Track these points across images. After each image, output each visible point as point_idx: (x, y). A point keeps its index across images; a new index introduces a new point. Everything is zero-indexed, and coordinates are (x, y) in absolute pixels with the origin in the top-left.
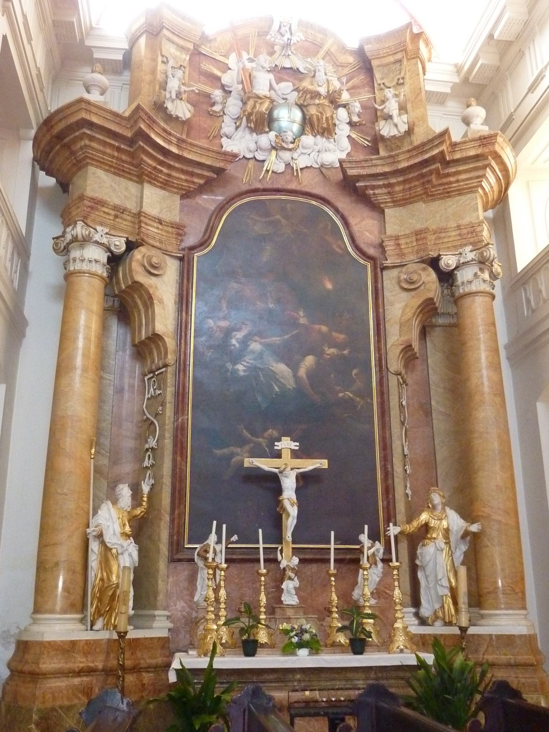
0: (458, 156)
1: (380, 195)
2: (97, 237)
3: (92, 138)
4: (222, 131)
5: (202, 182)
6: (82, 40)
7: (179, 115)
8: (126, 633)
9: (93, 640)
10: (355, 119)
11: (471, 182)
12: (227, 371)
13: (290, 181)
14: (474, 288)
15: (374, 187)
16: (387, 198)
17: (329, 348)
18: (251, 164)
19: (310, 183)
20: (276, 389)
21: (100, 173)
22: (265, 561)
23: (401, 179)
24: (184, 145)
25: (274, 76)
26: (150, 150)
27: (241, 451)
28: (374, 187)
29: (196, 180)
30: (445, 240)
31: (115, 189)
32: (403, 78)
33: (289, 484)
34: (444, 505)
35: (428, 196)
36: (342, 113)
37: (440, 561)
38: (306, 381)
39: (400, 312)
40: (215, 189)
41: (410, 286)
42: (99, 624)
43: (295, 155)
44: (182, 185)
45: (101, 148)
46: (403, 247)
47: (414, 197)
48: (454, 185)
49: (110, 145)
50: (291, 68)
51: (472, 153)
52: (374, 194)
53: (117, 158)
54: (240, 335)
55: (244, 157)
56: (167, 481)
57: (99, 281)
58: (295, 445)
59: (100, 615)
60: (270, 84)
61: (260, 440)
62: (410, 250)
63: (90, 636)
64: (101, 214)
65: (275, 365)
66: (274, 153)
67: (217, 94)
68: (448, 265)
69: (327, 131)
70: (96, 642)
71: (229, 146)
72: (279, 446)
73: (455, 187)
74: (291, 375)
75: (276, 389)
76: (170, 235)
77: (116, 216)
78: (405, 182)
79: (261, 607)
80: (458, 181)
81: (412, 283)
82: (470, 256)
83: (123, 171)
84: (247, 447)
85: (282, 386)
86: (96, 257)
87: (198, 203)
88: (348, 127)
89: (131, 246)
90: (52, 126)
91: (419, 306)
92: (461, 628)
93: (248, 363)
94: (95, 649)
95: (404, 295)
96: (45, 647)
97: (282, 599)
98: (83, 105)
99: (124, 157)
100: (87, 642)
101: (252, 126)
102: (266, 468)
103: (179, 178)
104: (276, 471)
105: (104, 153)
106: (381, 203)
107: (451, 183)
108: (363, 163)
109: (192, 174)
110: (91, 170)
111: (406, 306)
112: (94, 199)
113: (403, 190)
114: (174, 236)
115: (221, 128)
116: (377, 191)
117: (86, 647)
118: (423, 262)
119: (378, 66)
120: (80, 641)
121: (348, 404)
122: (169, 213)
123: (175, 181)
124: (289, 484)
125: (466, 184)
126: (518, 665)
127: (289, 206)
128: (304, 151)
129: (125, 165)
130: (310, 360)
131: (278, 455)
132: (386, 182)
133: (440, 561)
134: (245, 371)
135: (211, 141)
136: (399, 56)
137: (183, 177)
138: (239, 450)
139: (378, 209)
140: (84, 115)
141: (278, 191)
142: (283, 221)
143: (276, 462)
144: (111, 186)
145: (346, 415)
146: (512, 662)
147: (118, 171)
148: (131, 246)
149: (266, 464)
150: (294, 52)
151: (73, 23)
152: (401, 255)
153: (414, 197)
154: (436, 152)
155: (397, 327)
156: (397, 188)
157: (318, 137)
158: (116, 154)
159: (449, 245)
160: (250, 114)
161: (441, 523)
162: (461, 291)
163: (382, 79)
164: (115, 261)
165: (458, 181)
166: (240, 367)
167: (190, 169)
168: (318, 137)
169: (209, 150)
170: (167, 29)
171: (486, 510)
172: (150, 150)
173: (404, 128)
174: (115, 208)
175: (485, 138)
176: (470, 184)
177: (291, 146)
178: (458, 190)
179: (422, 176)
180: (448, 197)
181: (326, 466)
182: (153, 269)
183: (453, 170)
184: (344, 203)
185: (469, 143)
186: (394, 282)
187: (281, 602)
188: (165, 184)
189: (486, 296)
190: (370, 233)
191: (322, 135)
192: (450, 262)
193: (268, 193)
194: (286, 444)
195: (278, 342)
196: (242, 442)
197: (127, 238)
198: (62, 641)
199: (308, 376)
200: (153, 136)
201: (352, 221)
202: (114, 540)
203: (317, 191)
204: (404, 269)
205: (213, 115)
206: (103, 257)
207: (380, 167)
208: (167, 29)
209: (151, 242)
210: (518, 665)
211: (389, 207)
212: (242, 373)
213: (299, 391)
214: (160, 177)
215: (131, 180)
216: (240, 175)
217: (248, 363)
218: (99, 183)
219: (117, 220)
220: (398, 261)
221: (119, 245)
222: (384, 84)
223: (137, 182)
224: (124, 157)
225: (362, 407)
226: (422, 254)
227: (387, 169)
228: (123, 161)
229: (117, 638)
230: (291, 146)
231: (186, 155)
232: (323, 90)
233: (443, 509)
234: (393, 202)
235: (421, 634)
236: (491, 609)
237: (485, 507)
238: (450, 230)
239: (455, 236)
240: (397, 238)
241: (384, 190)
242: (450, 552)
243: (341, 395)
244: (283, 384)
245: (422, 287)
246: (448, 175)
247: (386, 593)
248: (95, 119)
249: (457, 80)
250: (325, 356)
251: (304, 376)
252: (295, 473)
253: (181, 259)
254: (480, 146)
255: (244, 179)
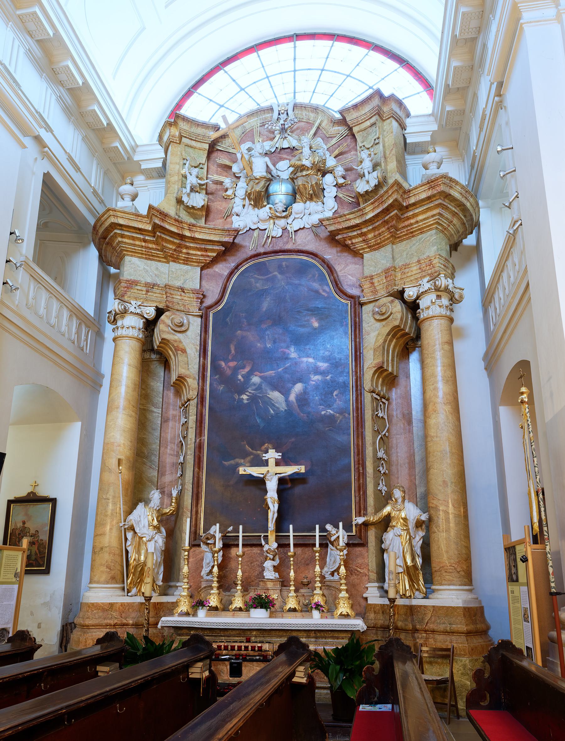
0: (412, 200)
1: (358, 243)
2: (132, 309)
3: (122, 236)
4: (233, 211)
5: (215, 254)
6: (130, 158)
7: (194, 205)
8: (150, 598)
9: (127, 603)
10: (341, 181)
11: (428, 221)
12: (235, 400)
13: (287, 242)
14: (431, 313)
15: (351, 238)
16: (363, 245)
17: (315, 375)
18: (256, 233)
19: (306, 241)
20: (272, 412)
21: (135, 260)
22: (243, 545)
23: (371, 227)
24: (194, 229)
25: (270, 159)
26: (168, 238)
27: (244, 462)
28: (351, 238)
29: (210, 254)
30: (409, 274)
31: (147, 271)
32: (378, 138)
33: (272, 486)
34: (404, 499)
35: (395, 238)
36: (329, 178)
37: (399, 546)
38: (296, 404)
39: (374, 339)
40: (228, 258)
41: (383, 317)
42: (134, 591)
43: (290, 220)
44: (200, 260)
45: (131, 242)
46: (376, 285)
47: (384, 241)
48: (415, 226)
49: (139, 239)
50: (289, 148)
51: (423, 196)
52: (352, 243)
53: (146, 247)
54: (245, 371)
55: (250, 228)
56: (189, 487)
57: (135, 342)
58: (278, 456)
59: (135, 585)
60: (267, 166)
61: (259, 452)
62: (381, 287)
63: (127, 600)
64: (136, 291)
65: (271, 393)
66: (272, 221)
67: (227, 181)
68: (409, 296)
69: (317, 194)
70: (130, 605)
71: (237, 223)
72: (266, 456)
73: (416, 227)
74: (284, 400)
75: (272, 412)
76: (192, 299)
77: (147, 291)
78: (374, 229)
79: (291, 581)
80: (417, 222)
81: (383, 314)
82: (427, 286)
83: (153, 256)
84: (249, 459)
85: (276, 409)
86: (133, 324)
87: (215, 271)
88: (335, 189)
89: (160, 312)
90: (97, 231)
91: (388, 334)
92: (390, 600)
93: (250, 393)
94: (128, 610)
95: (378, 324)
96: (89, 607)
97: (264, 574)
98: (111, 213)
99: (150, 246)
100: (122, 604)
101: (253, 203)
102: (255, 474)
103: (196, 255)
104: (262, 476)
105: (134, 245)
106: (360, 250)
107: (412, 224)
108: (339, 219)
109: (206, 250)
110: (127, 259)
111: (379, 334)
112: (128, 281)
113: (375, 236)
114: (195, 300)
115: (233, 207)
116: (354, 241)
117: (121, 608)
118: (391, 295)
119: (359, 132)
120: (117, 603)
121: (331, 419)
122: (191, 283)
123: (194, 257)
124: (272, 486)
125: (424, 224)
126: (453, 633)
127: (284, 264)
128: (297, 216)
129: (153, 251)
130: (299, 387)
131: (265, 463)
132: (359, 232)
133: (399, 546)
134: (248, 400)
135: (226, 220)
136: (373, 120)
137: (199, 253)
138: (242, 461)
139: (357, 254)
140: (112, 220)
141: (276, 252)
142: (279, 276)
143: (263, 470)
144: (144, 268)
145: (327, 429)
146: (448, 629)
147: (149, 256)
148: (160, 312)
149: (256, 471)
150: (290, 134)
151: (117, 147)
152: (375, 292)
153: (384, 241)
154: (391, 201)
155: (372, 352)
156: (370, 236)
157: (308, 202)
158: (143, 244)
159: (412, 278)
160: (250, 194)
161: (400, 513)
162: (422, 316)
163: (363, 142)
164: (150, 325)
165: (417, 222)
166: (245, 397)
167: (203, 246)
168: (308, 202)
169: (215, 229)
170: (186, 137)
171: (435, 502)
172: (168, 238)
173: (373, 183)
174: (147, 285)
175: (432, 182)
176: (427, 223)
177: (284, 214)
178: (419, 229)
179: (386, 222)
180: (413, 236)
181: (303, 471)
182: (180, 328)
183: (411, 213)
184: (330, 254)
185: (421, 188)
186: (370, 315)
187: (264, 577)
188: (187, 261)
189: (441, 319)
190: (352, 277)
191: (311, 199)
192: (411, 293)
193: (269, 255)
194: (272, 455)
195: (273, 375)
196: (245, 455)
197: (156, 307)
198: (102, 603)
199: (296, 400)
200: (167, 226)
201: (338, 268)
202: (145, 530)
203: (310, 247)
204: (377, 303)
205: (226, 199)
206: (140, 323)
207: (342, 224)
208: (186, 137)
209: (177, 307)
210: (453, 633)
211: (368, 252)
212: (245, 402)
213: (289, 412)
214: (181, 256)
215: (160, 261)
216: (248, 244)
217: (250, 393)
218: (135, 267)
219: (149, 294)
220: (372, 298)
221: (150, 312)
222: (364, 146)
223: (165, 262)
224: (150, 246)
225: (341, 421)
226: (390, 289)
227: (358, 221)
228: (150, 249)
229: (144, 601)
230: (284, 214)
231: (197, 236)
232: (307, 163)
233: (403, 501)
234: (369, 247)
235: (381, 604)
236: (437, 585)
237: (433, 499)
238: (412, 265)
239: (417, 270)
240: (372, 278)
241: (360, 239)
242: (408, 537)
243: (323, 413)
244: (278, 408)
245: (391, 317)
246: (408, 218)
247: (358, 571)
248: (121, 221)
249: (435, 127)
250: (311, 382)
251: (295, 401)
252: (277, 478)
253: (201, 317)
254: (429, 189)
255: (250, 246)
